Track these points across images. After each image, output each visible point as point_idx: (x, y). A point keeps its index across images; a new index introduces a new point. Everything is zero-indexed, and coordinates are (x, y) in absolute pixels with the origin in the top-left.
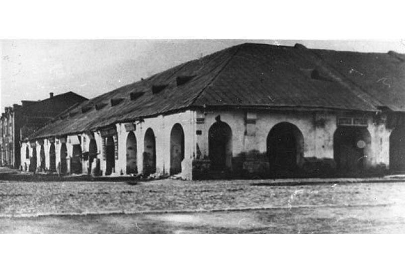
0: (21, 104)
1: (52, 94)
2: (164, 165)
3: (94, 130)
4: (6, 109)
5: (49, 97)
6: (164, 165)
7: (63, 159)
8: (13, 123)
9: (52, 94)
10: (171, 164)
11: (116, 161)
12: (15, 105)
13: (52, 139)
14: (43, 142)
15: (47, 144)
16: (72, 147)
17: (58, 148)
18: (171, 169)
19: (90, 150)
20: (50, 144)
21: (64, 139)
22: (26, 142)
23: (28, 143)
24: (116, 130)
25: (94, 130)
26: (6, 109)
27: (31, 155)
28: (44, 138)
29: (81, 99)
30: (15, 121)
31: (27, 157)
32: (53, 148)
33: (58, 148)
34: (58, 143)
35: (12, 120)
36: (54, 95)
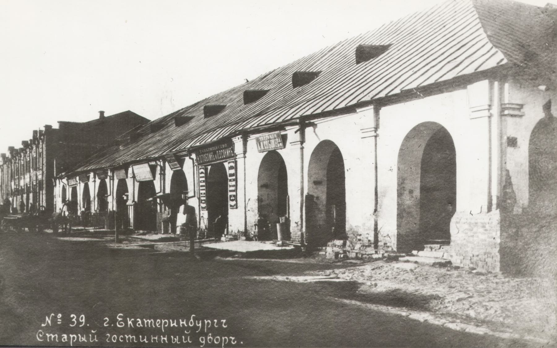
0: (56, 126)
1: (102, 113)
2: (376, 225)
3: (184, 153)
4: (35, 132)
5: (97, 117)
6: (376, 225)
7: (121, 203)
8: (44, 153)
9: (102, 113)
10: (399, 226)
11: (231, 211)
12: (48, 127)
13: (102, 173)
14: (88, 178)
15: (95, 181)
16: (509, 147)
17: (112, 186)
18: (400, 237)
19: (171, 190)
20: (98, 181)
21: (123, 171)
22: (61, 178)
23: (65, 180)
24: (233, 150)
25: (184, 153)
26: (35, 132)
27: (69, 196)
28: (89, 171)
29: (143, 120)
30: (47, 150)
31: (64, 200)
32: (103, 188)
33: (112, 186)
34: (112, 178)
35: (43, 147)
36: (106, 115)
